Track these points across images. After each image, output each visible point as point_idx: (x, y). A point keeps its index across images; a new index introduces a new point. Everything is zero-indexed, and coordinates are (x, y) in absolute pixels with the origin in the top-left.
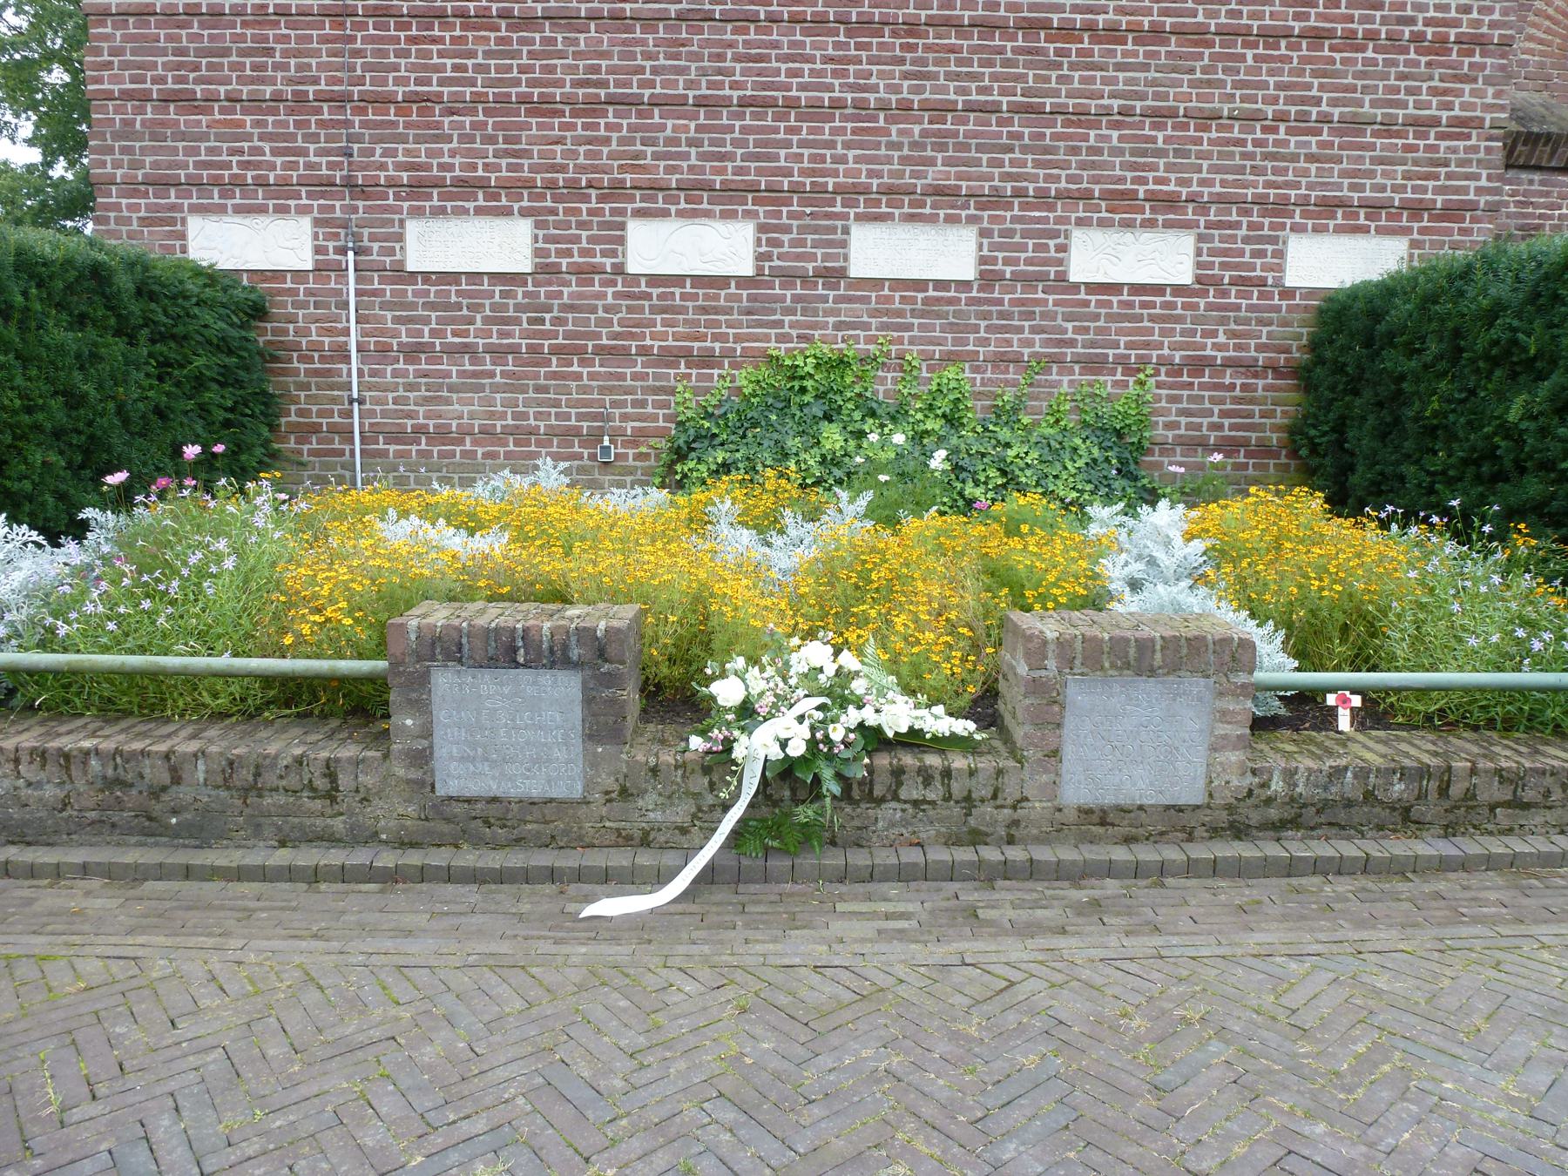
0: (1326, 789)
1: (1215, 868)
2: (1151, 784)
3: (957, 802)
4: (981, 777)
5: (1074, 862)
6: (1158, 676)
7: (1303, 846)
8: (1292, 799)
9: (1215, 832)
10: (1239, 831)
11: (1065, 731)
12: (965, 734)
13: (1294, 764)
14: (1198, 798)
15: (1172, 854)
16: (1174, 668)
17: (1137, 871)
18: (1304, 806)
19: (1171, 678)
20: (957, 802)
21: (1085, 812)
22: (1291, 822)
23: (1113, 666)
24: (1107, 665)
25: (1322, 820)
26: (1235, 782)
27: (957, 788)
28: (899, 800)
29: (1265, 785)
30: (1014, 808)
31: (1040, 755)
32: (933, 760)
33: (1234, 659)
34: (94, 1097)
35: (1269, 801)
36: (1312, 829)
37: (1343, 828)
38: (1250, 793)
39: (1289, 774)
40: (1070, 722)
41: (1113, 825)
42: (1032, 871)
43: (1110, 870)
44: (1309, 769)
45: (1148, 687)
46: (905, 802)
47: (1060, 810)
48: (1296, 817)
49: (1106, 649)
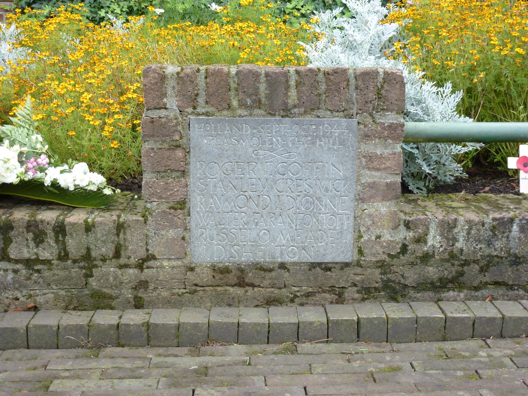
0: (489, 244)
1: (359, 331)
2: (293, 240)
3: (75, 261)
4: (99, 232)
5: (196, 326)
6: (294, 115)
7: (463, 306)
8: (452, 256)
9: (367, 293)
10: (394, 292)
11: (191, 180)
12: (94, 188)
13: (454, 216)
14: (347, 255)
15: (312, 315)
16: (311, 107)
17: (269, 335)
18: (466, 263)
19: (308, 118)
20: (75, 261)
21: (221, 271)
22: (452, 281)
23: (242, 104)
24: (235, 103)
25: (487, 279)
26: (387, 237)
27: (74, 245)
28: (9, 260)
29: (420, 240)
30: (140, 266)
31: (164, 207)
32: (48, 216)
33: (379, 96)
34: (501, 336)
35: (426, 258)
36: (476, 289)
37: (511, 287)
38: (404, 249)
39: (448, 228)
40: (196, 169)
41: (253, 286)
42: (150, 336)
43: (238, 334)
44: (469, 222)
45: (282, 129)
46: (17, 261)
47: (192, 269)
48: (456, 276)
49: (233, 85)
